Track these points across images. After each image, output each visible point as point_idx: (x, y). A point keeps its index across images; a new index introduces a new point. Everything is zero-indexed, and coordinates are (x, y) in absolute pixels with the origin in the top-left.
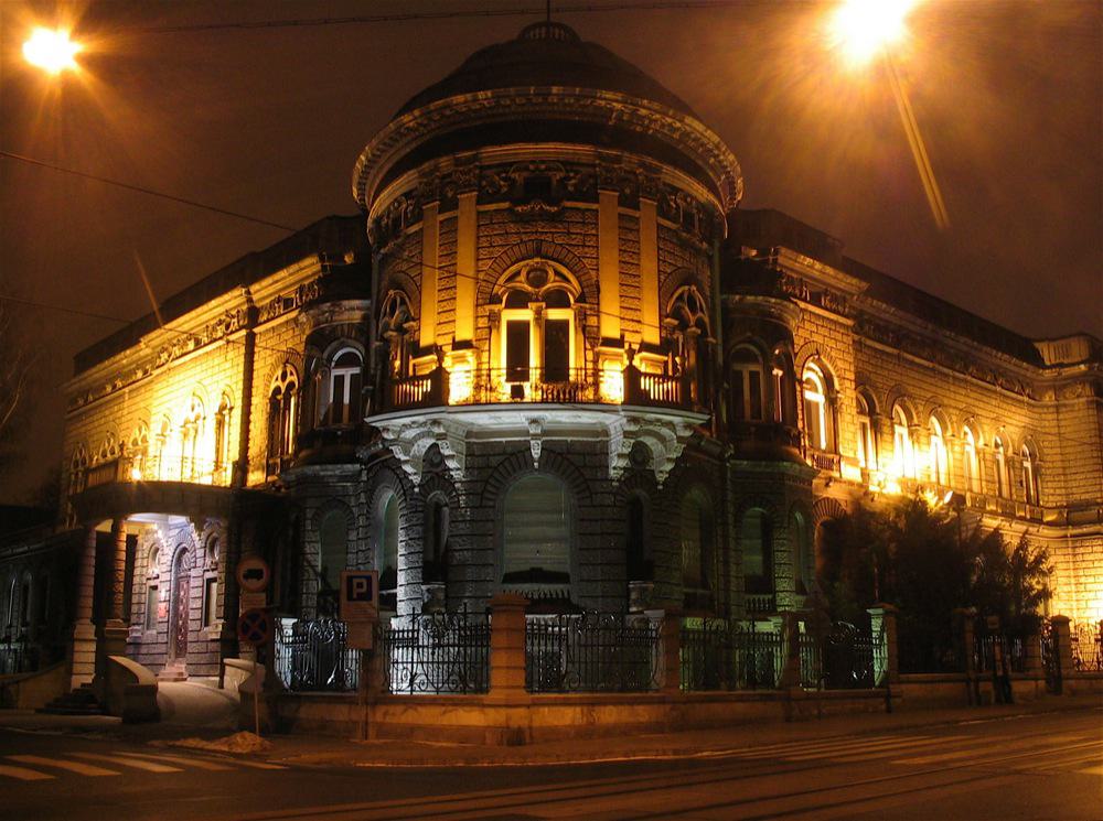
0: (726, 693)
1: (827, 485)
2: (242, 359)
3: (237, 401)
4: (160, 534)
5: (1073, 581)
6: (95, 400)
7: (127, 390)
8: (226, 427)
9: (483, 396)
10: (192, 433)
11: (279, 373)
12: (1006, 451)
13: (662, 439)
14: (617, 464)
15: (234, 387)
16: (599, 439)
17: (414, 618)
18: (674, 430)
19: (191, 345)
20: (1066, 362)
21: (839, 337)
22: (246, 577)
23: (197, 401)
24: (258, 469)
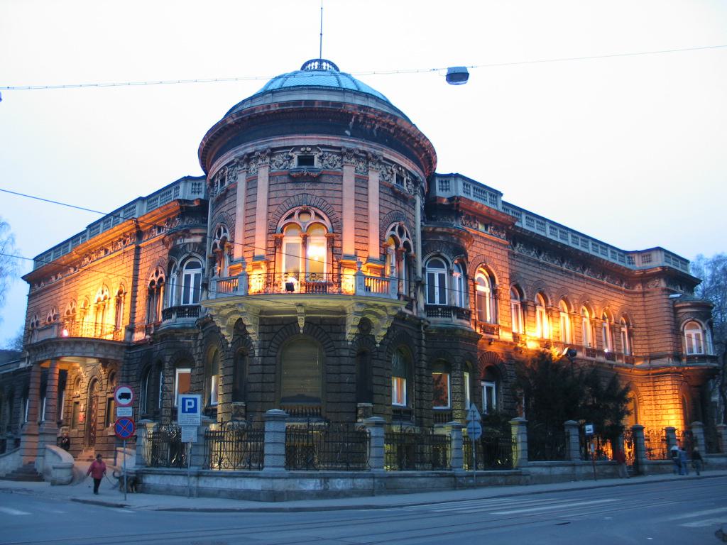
0: (483, 471)
1: (490, 344)
3: (128, 289)
4: (81, 369)
5: (653, 402)
8: (122, 304)
9: (270, 290)
10: (102, 307)
12: (610, 321)
13: (379, 316)
14: (351, 331)
16: (340, 316)
17: (222, 424)
18: (386, 310)
21: (499, 251)
22: (120, 397)
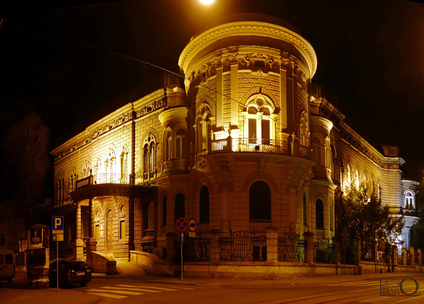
2: (131, 133)
6: (66, 155)
7: (79, 150)
11: (147, 138)
15: (128, 144)
19: (108, 129)
20: (391, 155)
23: (111, 151)
24: (139, 177)
